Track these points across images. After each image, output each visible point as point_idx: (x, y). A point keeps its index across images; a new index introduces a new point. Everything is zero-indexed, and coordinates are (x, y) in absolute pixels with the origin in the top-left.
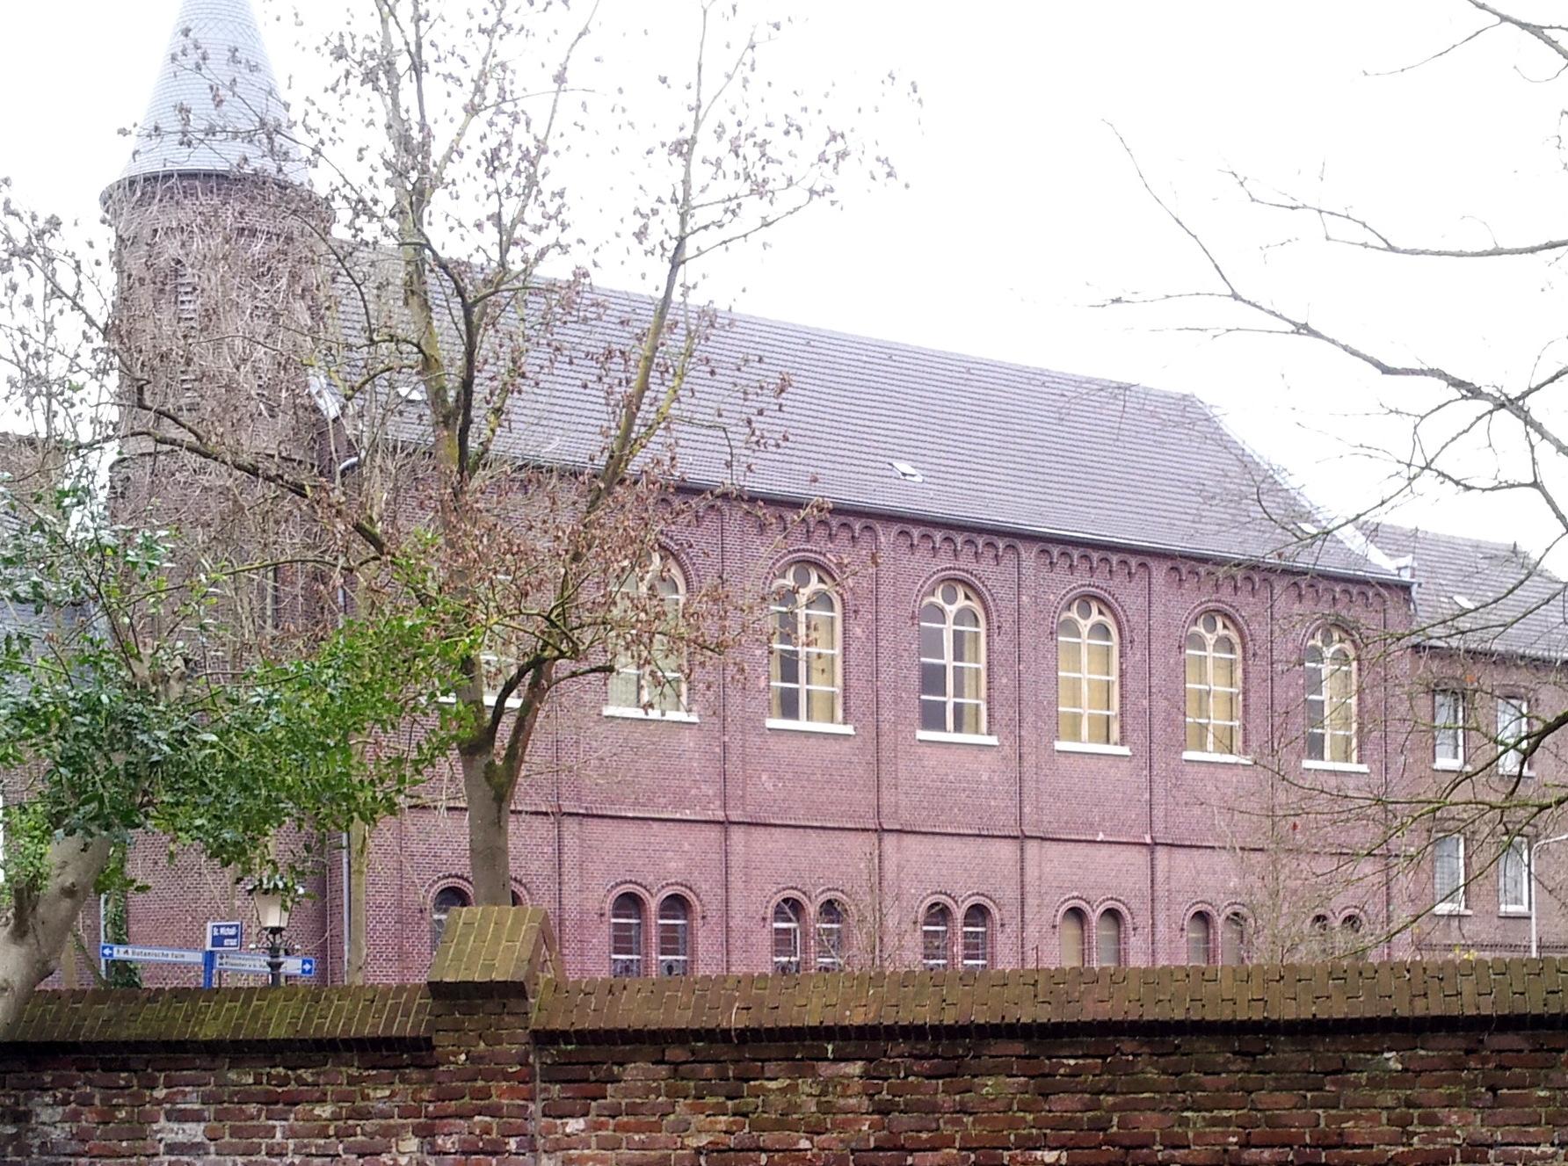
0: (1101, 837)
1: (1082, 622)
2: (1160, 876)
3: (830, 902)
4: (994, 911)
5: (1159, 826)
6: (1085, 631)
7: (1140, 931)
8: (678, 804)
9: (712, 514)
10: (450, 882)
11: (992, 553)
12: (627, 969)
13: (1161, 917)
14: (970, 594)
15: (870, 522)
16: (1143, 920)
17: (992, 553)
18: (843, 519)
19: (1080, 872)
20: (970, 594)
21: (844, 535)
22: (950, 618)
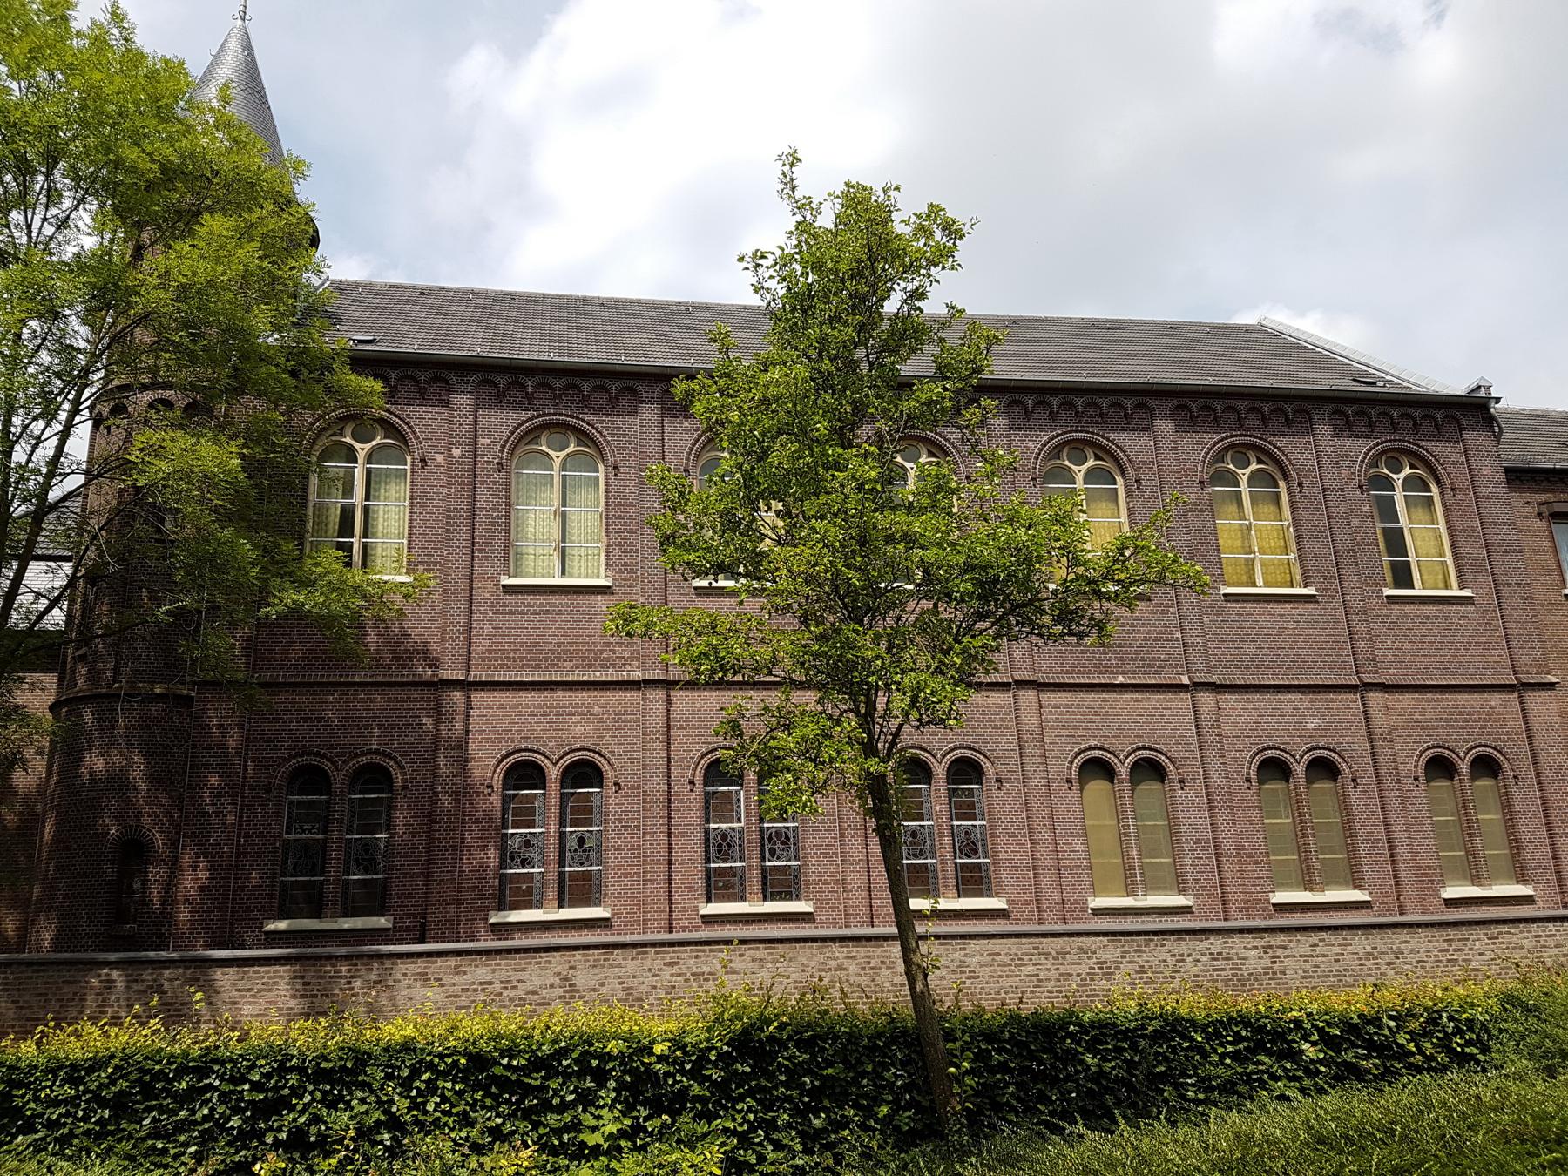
0: (1120, 680)
1: (1075, 468)
2: (1206, 721)
3: (716, 762)
4: (986, 765)
5: (1197, 664)
6: (1080, 478)
7: (1362, 782)
8: (590, 666)
9: (1141, 412)
10: (575, 756)
11: (1234, 416)
12: (528, 844)
13: (1214, 765)
14: (1263, 458)
15: (631, 383)
16: (1193, 769)
17: (1234, 416)
18: (1115, 399)
19: (1097, 719)
20: (1263, 458)
21: (1385, 422)
22: (557, 464)
